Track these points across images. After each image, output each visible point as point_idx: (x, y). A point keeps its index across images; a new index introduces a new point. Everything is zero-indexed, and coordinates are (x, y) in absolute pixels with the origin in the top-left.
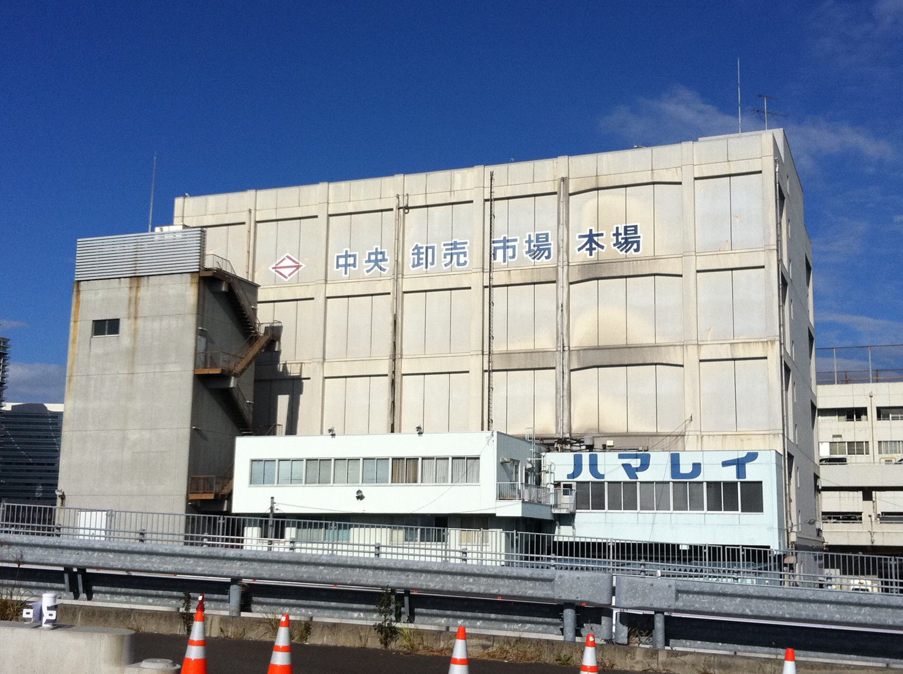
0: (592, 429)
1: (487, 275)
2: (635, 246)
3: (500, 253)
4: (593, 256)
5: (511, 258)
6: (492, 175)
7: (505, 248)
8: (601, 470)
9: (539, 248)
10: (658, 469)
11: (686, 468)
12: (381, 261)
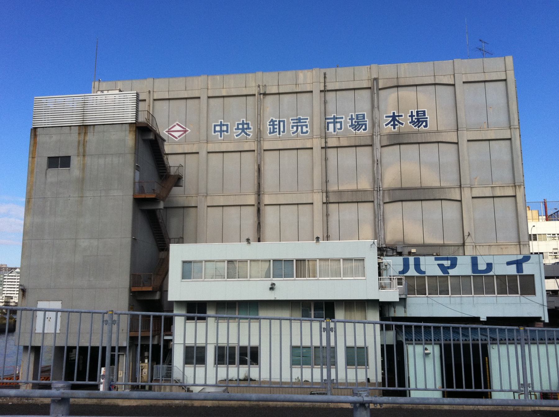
0: (399, 242)
1: (323, 140)
2: (424, 124)
3: (331, 126)
4: (396, 130)
5: (339, 129)
6: (325, 74)
7: (335, 123)
8: (422, 268)
9: (358, 124)
10: (463, 268)
11: (482, 266)
12: (246, 129)
